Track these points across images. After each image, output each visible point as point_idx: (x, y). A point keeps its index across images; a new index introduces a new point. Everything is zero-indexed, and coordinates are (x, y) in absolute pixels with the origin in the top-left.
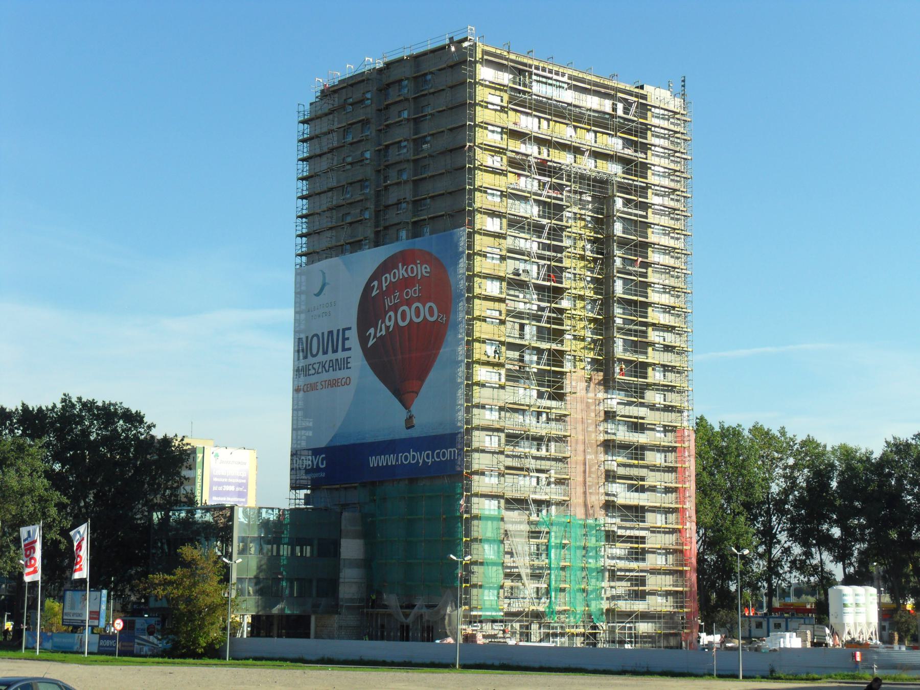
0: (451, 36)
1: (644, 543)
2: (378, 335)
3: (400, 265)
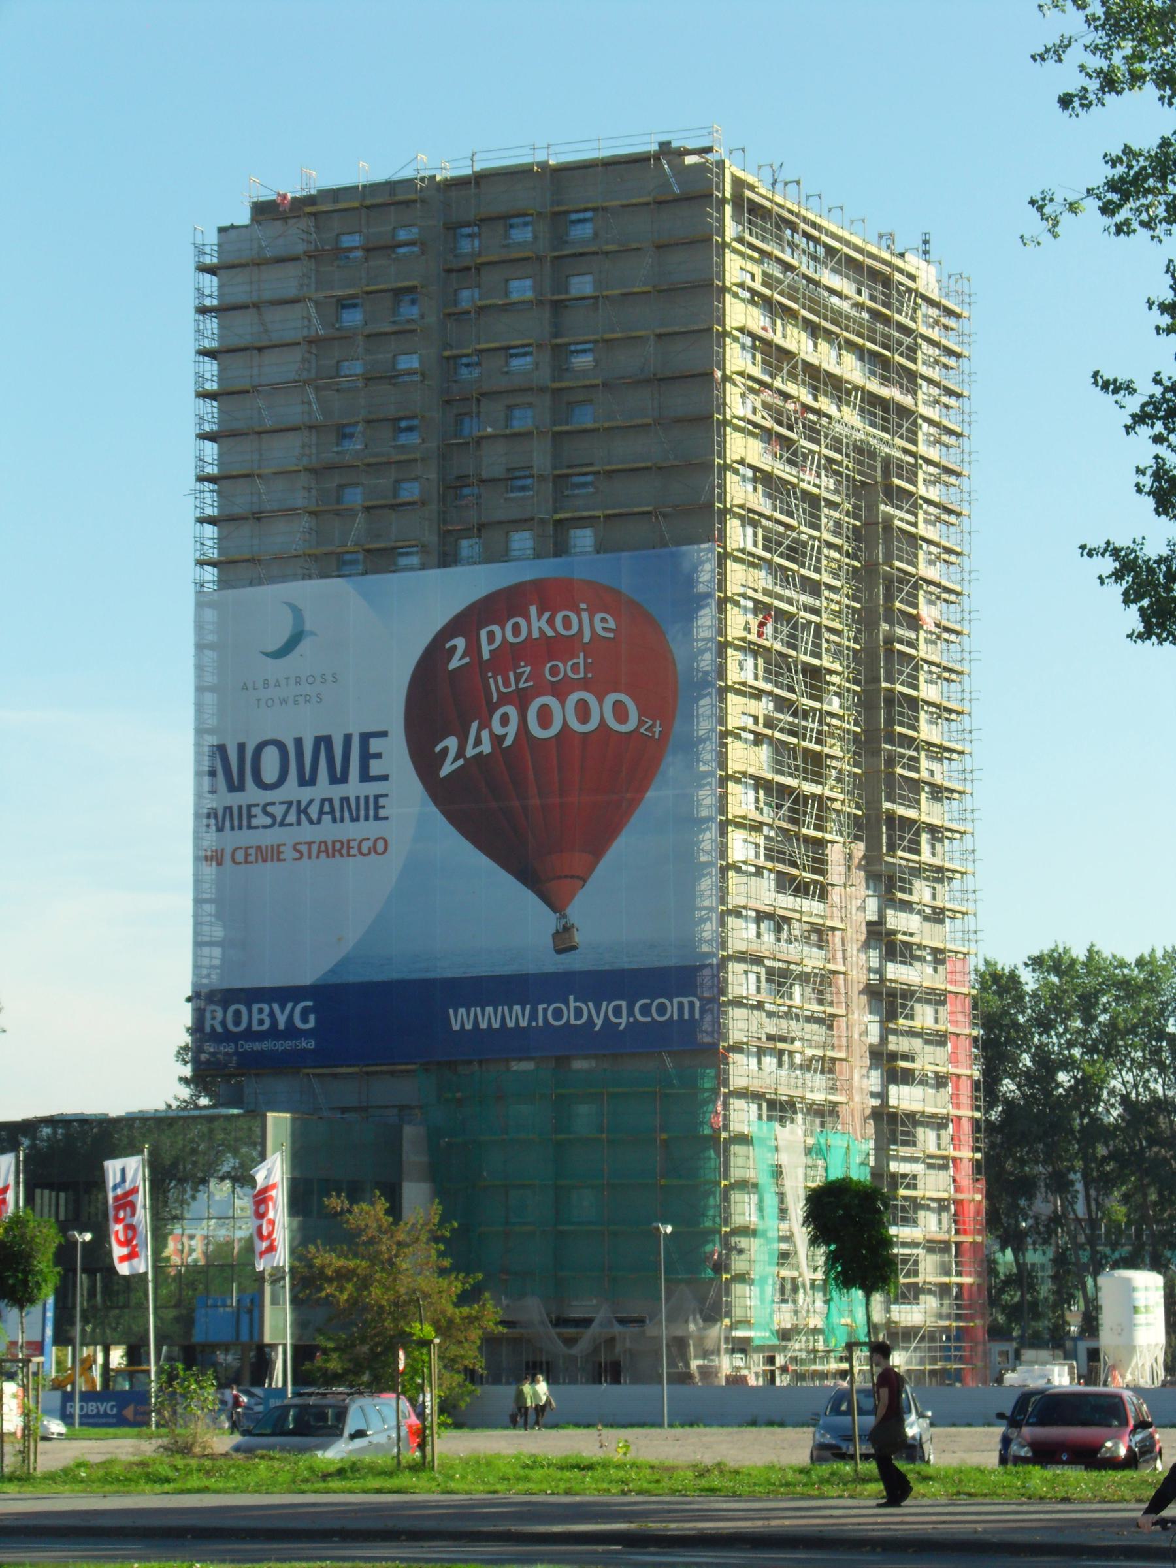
0: (664, 138)
1: (915, 1187)
2: (470, 752)
3: (533, 610)
